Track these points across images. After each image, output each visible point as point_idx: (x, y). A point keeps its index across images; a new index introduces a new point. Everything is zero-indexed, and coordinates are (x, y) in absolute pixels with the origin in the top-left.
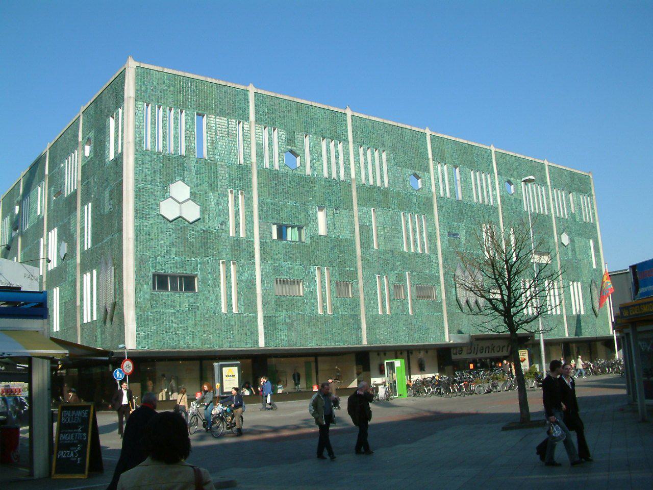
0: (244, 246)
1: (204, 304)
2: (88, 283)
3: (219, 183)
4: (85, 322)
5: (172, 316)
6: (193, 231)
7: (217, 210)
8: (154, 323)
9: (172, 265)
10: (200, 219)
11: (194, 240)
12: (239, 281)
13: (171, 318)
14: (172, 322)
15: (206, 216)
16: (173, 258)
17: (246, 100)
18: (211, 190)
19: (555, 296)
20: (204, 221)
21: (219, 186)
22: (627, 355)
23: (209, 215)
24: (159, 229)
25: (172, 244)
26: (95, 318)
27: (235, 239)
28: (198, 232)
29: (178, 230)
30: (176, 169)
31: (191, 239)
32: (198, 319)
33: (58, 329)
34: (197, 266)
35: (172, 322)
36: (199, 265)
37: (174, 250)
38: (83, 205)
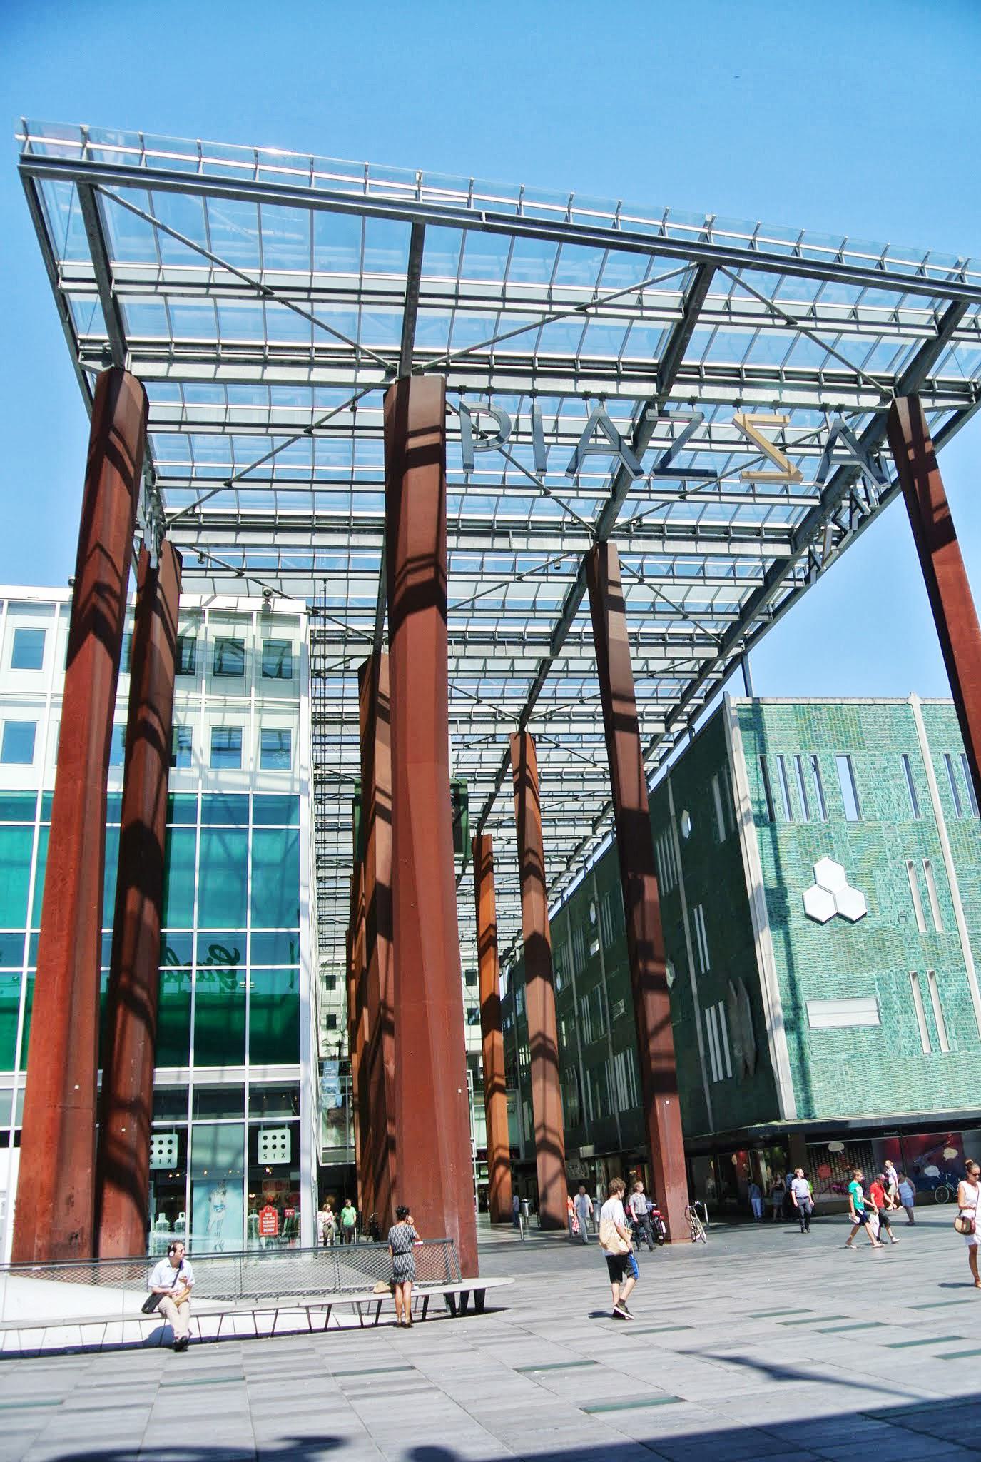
0: (944, 943)
1: (893, 1042)
2: (712, 1021)
3: (888, 853)
6: (859, 931)
7: (892, 895)
8: (819, 1077)
9: (835, 988)
10: (865, 915)
12: (943, 1001)
14: (847, 1074)
15: (876, 907)
16: (835, 976)
17: (910, 719)
19: (341, 744)
21: (889, 858)
22: (732, 816)
23: (880, 904)
24: (809, 936)
26: (730, 1074)
27: (928, 935)
32: (886, 1066)
34: (873, 983)
35: (847, 1074)
36: (876, 983)
37: (834, 963)
38: (691, 905)
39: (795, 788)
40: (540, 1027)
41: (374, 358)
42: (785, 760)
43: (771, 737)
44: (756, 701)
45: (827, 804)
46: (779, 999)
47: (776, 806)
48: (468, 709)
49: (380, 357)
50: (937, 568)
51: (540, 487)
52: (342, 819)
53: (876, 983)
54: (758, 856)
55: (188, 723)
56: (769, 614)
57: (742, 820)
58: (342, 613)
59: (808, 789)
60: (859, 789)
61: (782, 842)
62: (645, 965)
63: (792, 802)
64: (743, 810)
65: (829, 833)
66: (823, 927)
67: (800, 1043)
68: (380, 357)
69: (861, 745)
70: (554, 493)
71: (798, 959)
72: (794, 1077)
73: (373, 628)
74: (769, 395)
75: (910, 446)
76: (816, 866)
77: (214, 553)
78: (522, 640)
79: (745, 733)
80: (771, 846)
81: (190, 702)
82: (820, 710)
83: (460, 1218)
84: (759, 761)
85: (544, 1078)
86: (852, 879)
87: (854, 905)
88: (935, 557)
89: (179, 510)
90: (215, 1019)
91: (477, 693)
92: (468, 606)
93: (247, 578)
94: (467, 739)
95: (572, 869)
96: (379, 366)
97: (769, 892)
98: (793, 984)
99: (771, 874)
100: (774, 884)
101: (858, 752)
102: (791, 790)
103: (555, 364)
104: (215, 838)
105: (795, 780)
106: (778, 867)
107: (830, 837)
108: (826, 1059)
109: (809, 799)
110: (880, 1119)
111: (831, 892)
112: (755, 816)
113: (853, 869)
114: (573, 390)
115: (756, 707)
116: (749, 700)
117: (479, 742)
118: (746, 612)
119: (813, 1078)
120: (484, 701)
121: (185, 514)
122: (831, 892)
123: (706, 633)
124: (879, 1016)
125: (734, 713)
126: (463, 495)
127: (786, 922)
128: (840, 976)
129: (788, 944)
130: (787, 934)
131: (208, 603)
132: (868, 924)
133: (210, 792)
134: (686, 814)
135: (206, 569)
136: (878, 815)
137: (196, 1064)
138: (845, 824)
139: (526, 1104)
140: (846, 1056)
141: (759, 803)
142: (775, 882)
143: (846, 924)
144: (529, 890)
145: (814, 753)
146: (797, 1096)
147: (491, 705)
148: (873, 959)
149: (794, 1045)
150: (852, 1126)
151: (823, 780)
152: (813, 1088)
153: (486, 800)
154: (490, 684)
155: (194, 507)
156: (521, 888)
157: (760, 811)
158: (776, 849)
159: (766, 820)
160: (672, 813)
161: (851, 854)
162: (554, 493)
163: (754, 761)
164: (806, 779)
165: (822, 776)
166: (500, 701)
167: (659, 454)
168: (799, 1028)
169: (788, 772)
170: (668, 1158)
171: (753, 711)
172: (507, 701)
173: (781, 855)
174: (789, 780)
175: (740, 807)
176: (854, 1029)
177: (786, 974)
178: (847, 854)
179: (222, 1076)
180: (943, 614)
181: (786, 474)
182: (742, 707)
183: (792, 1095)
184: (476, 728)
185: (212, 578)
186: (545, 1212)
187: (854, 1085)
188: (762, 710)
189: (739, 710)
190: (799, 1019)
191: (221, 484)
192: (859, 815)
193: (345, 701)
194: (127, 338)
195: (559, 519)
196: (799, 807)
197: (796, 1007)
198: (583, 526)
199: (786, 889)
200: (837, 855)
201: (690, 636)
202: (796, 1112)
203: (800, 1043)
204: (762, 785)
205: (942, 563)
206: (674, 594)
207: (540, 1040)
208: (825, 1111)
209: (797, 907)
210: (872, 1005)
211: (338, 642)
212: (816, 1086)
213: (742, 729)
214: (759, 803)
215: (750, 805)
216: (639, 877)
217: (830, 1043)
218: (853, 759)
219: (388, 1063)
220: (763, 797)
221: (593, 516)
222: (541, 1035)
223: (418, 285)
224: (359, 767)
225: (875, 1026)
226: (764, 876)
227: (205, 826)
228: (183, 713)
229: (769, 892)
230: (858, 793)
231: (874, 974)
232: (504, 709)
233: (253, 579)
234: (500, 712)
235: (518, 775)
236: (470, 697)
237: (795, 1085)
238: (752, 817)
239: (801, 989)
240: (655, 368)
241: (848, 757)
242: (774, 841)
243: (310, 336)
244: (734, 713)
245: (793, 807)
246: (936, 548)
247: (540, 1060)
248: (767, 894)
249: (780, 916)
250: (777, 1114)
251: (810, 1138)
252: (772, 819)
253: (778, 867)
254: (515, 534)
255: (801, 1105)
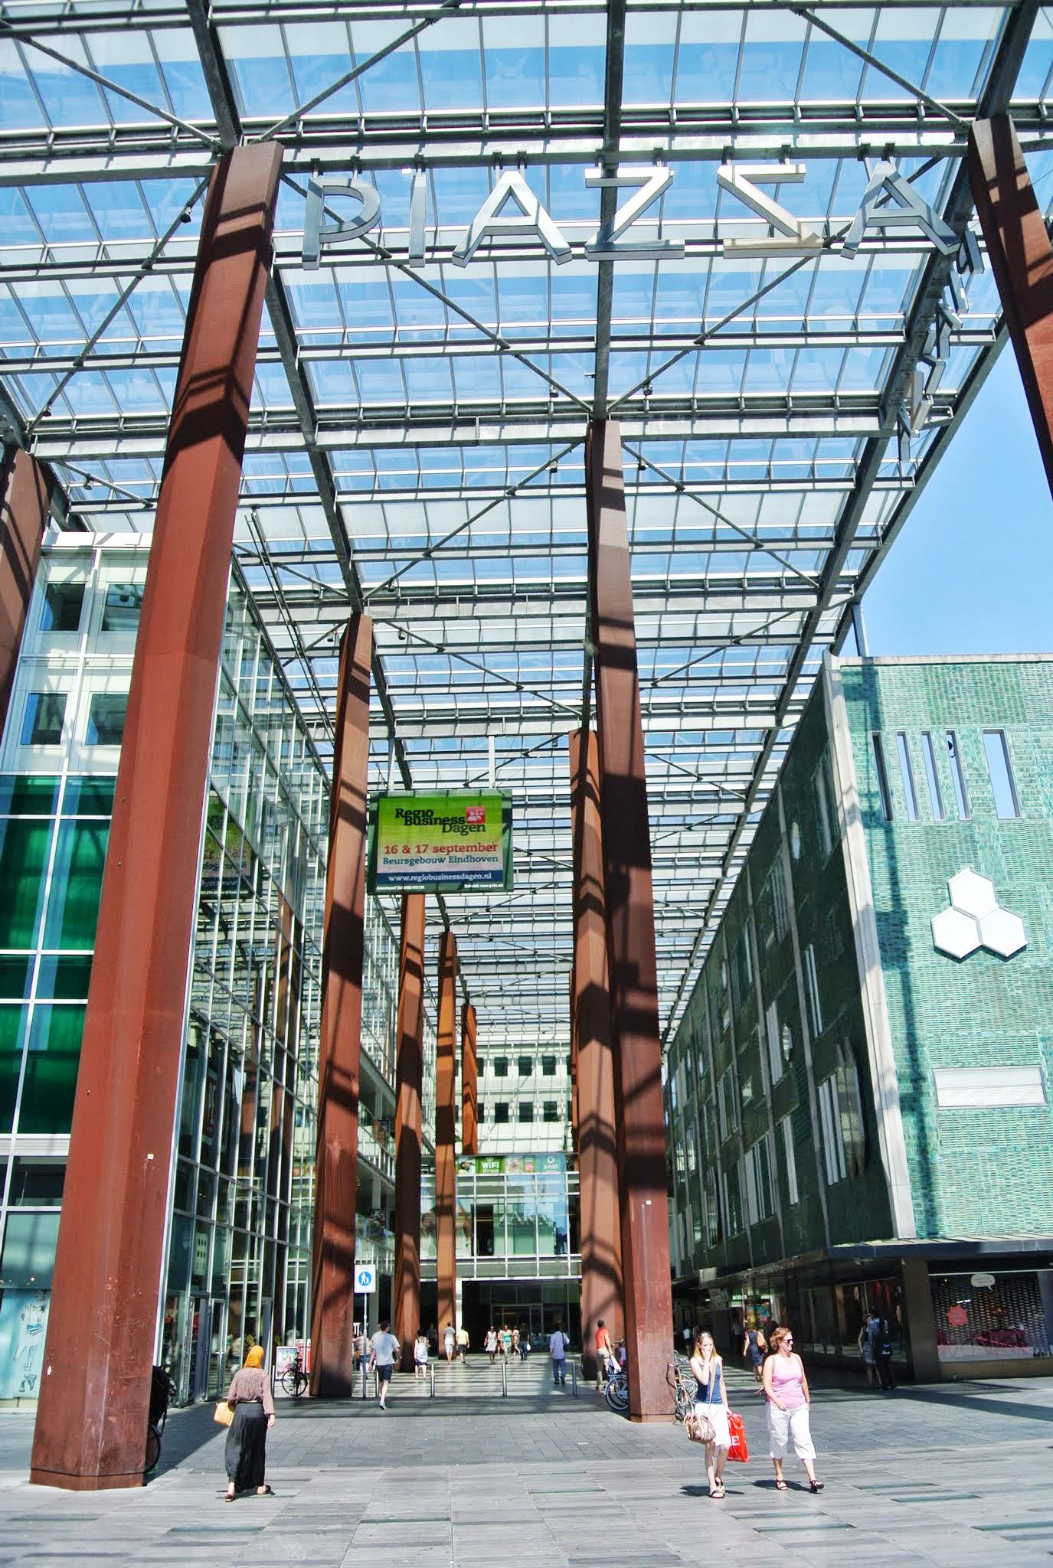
4: (830, 1183)
5: (991, 1161)
6: (1015, 971)
10: (1023, 949)
11: (1020, 992)
13: (988, 1167)
14: (994, 1174)
15: (1041, 938)
16: (979, 1034)
18: (1044, 880)
20: (1038, 948)
25: (972, 1006)
26: (844, 1175)
28: (1027, 971)
29: (981, 973)
30: (958, 849)
31: (1012, 991)
33: (797, 1201)
34: (1036, 1046)
35: (994, 1174)
36: (1040, 1045)
37: (976, 1016)
38: (803, 947)
39: (922, 775)
40: (593, 1106)
41: (196, 135)
42: (908, 738)
43: (889, 708)
44: (869, 662)
45: (969, 797)
46: (893, 1066)
47: (894, 801)
48: (688, 788)
49: (206, 135)
50: (1033, 349)
51: (494, 340)
52: (559, 910)
53: (1040, 1045)
54: (866, 868)
55: (61, 690)
56: (877, 539)
57: (844, 820)
58: (547, 687)
59: (941, 777)
60: (1017, 775)
61: (901, 850)
62: (624, 996)
63: (918, 794)
64: (847, 805)
65: (972, 837)
66: (961, 966)
67: (922, 1129)
68: (206, 135)
69: (1021, 716)
70: (514, 347)
71: (921, 1011)
72: (912, 1176)
73: (581, 703)
74: (775, 141)
75: (994, 183)
76: (950, 881)
77: (414, 628)
78: (743, 709)
79: (853, 703)
80: (884, 854)
81: (67, 664)
82: (961, 670)
83: (114, 1372)
84: (871, 740)
85: (595, 1173)
86: (1006, 899)
87: (1007, 934)
88: (1030, 333)
89: (376, 585)
90: (47, 1069)
91: (697, 771)
92: (682, 675)
93: (448, 654)
94: (688, 820)
95: (710, 925)
96: (204, 146)
97: (881, 917)
98: (912, 1046)
99: (885, 891)
100: (888, 907)
101: (1015, 726)
102: (916, 778)
103: (455, 123)
104: (86, 836)
105: (922, 764)
106: (894, 882)
107: (973, 841)
108: (962, 1153)
109: (943, 791)
110: (1033, 1242)
111: (973, 917)
112: (864, 814)
113: (1008, 885)
114: (784, 430)
115: (868, 671)
116: (859, 661)
117: (702, 824)
118: (843, 532)
119: (941, 1180)
120: (705, 779)
121: (382, 588)
122: (973, 917)
123: (800, 577)
124: (1045, 1093)
125: (837, 677)
126: (670, 553)
127: (905, 959)
128: (985, 1034)
129: (907, 989)
130: (905, 975)
131: (102, 542)
132: (1027, 961)
133: (77, 774)
134: (795, 827)
135: (406, 646)
136: (1045, 810)
137: (20, 1131)
138: (996, 824)
139: (681, 1215)
140: (992, 1149)
141: (869, 795)
142: (890, 903)
143: (996, 961)
144: (586, 929)
145: (951, 728)
146: (918, 1205)
147: (711, 783)
148: (1035, 1011)
149: (913, 1131)
150: (987, 1250)
151: (964, 765)
152: (941, 1193)
153: (713, 887)
154: (713, 760)
155: (390, 582)
156: (575, 927)
157: (871, 807)
158: (892, 857)
159: (880, 820)
160: (783, 828)
161: (1003, 863)
162: (514, 347)
163: (863, 741)
164: (939, 764)
165: (962, 758)
166: (722, 778)
167: (898, 496)
168: (921, 1107)
169: (912, 754)
170: (643, 1288)
171: (863, 674)
172: (730, 778)
173: (900, 866)
174: (914, 766)
175: (842, 802)
176: (1004, 1111)
177: (902, 1033)
178: (999, 864)
179: (51, 1147)
180: (1045, 421)
181: (794, 240)
182: (848, 669)
183: (910, 1203)
184: (698, 809)
185: (414, 655)
186: (588, 1352)
187: (1006, 1188)
188: (876, 673)
189: (845, 674)
190: (921, 1094)
191: (420, 555)
192: (1017, 813)
193: (556, 782)
194: (316, 407)
195: (778, 574)
196: (928, 801)
197: (917, 1078)
198: (579, 407)
199: (905, 912)
200: (983, 866)
201: (778, 581)
202: (915, 1229)
203: (922, 1129)
204: (874, 772)
205: (1038, 342)
206: (740, 510)
207: (593, 1123)
208: (954, 1228)
209: (923, 937)
210: (1034, 1076)
211: (311, 605)
212: (944, 1193)
213: (847, 698)
214: (869, 795)
215: (857, 800)
216: (624, 870)
217: (969, 1128)
218: (1008, 735)
219: (331, 1142)
220: (875, 787)
221: (816, 569)
222: (595, 1116)
223: (608, 326)
224: (571, 852)
225: (1038, 1106)
226: (874, 895)
227: (66, 817)
228: (57, 677)
229: (881, 917)
230: (1016, 781)
231: (1037, 1031)
232: (727, 786)
233: (455, 655)
234: (723, 790)
235: (575, 785)
236: (690, 775)
237: (914, 1190)
238: (858, 815)
239: (926, 1053)
240: (601, 118)
241: (1001, 733)
242: (890, 847)
243: (499, 392)
244: (837, 677)
245: (919, 801)
246: (1032, 321)
247: (591, 1149)
248: (879, 920)
249: (897, 950)
250: (888, 1231)
251: (934, 1266)
252: (889, 817)
253: (894, 882)
254: (482, 422)
255: (922, 1217)
